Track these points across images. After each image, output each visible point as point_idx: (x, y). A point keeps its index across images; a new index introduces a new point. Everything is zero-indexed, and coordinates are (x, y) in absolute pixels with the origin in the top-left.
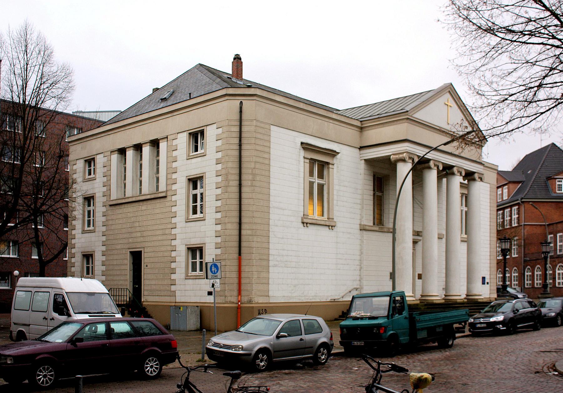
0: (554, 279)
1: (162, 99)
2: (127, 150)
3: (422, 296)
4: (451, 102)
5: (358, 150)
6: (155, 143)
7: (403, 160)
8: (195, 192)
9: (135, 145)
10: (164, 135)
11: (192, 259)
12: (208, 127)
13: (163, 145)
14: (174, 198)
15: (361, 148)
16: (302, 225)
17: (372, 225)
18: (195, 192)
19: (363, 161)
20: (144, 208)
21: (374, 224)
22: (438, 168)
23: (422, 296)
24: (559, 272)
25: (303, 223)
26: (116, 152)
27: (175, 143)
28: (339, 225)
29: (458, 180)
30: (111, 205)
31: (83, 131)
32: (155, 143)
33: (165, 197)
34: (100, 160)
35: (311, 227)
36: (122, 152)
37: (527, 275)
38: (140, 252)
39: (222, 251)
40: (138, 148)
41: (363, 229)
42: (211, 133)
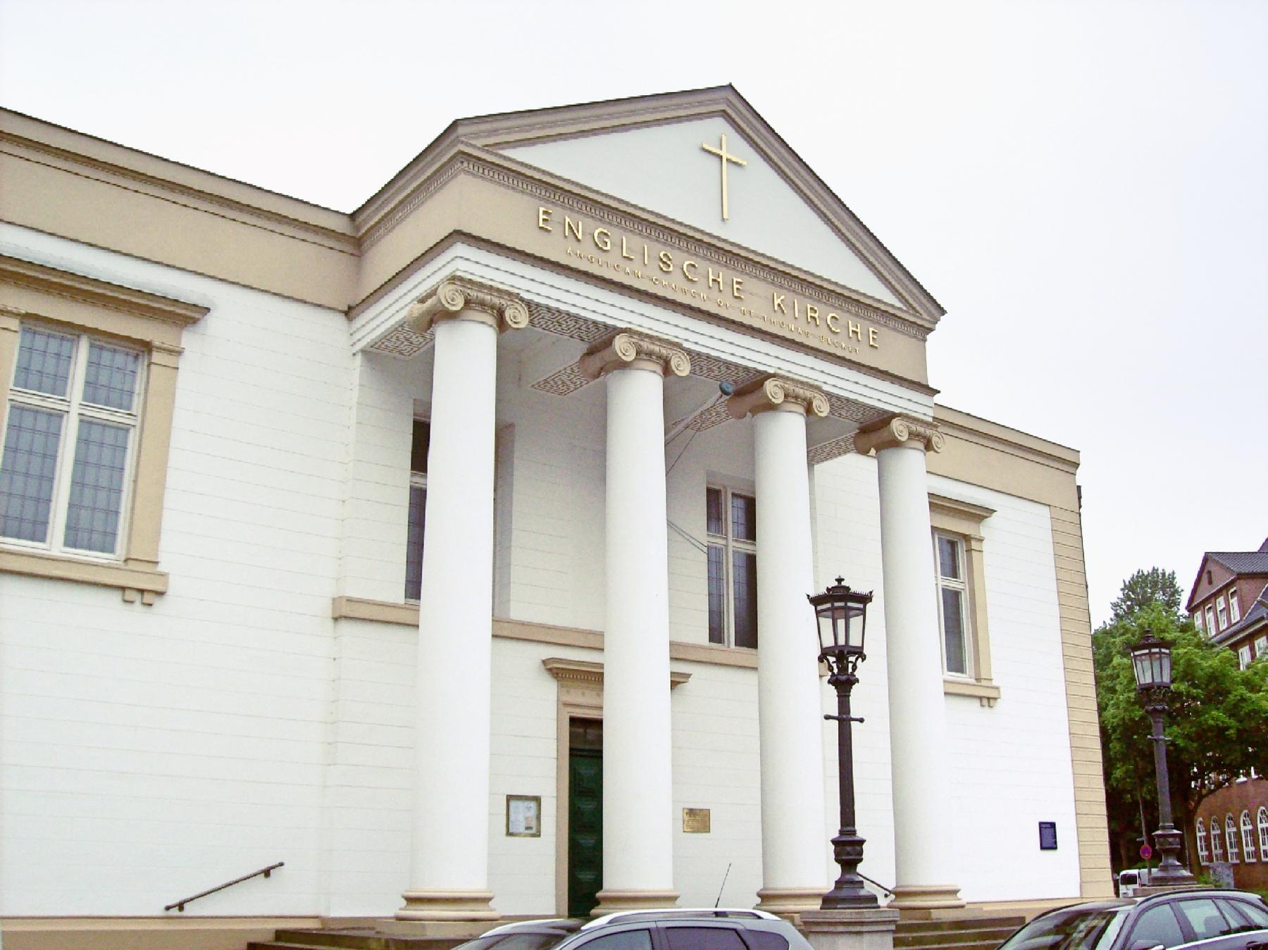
0: (1239, 844)
4: (734, 146)
5: (341, 319)
15: (349, 313)
17: (397, 594)
19: (359, 357)
21: (716, 634)
22: (809, 410)
28: (175, 586)
29: (639, 403)
37: (1262, 830)
38: (1053, 825)
41: (346, 613)
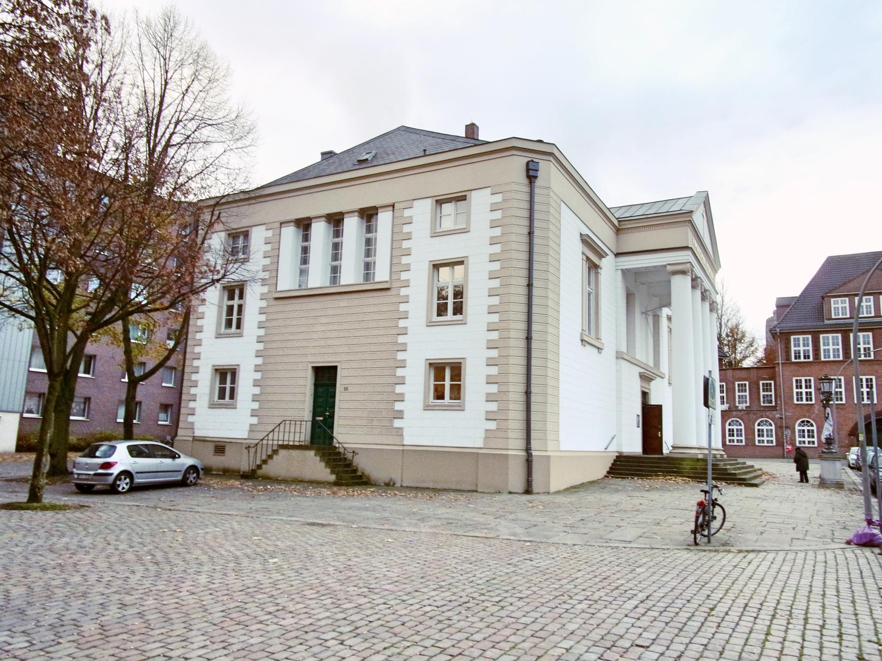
1: (358, 161)
2: (380, 210)
3: (674, 447)
6: (368, 215)
7: (683, 272)
8: (231, 303)
9: (361, 209)
10: (389, 201)
11: (435, 380)
12: (254, 229)
13: (384, 219)
14: (403, 292)
16: (580, 342)
18: (231, 303)
20: (343, 304)
23: (674, 447)
24: (760, 427)
25: (582, 340)
26: (293, 224)
27: (407, 213)
30: (276, 299)
31: (427, 153)
32: (368, 215)
33: (388, 289)
34: (258, 238)
35: (588, 347)
36: (304, 225)
38: (334, 369)
39: (499, 370)
40: (336, 220)
42: (481, 201)
